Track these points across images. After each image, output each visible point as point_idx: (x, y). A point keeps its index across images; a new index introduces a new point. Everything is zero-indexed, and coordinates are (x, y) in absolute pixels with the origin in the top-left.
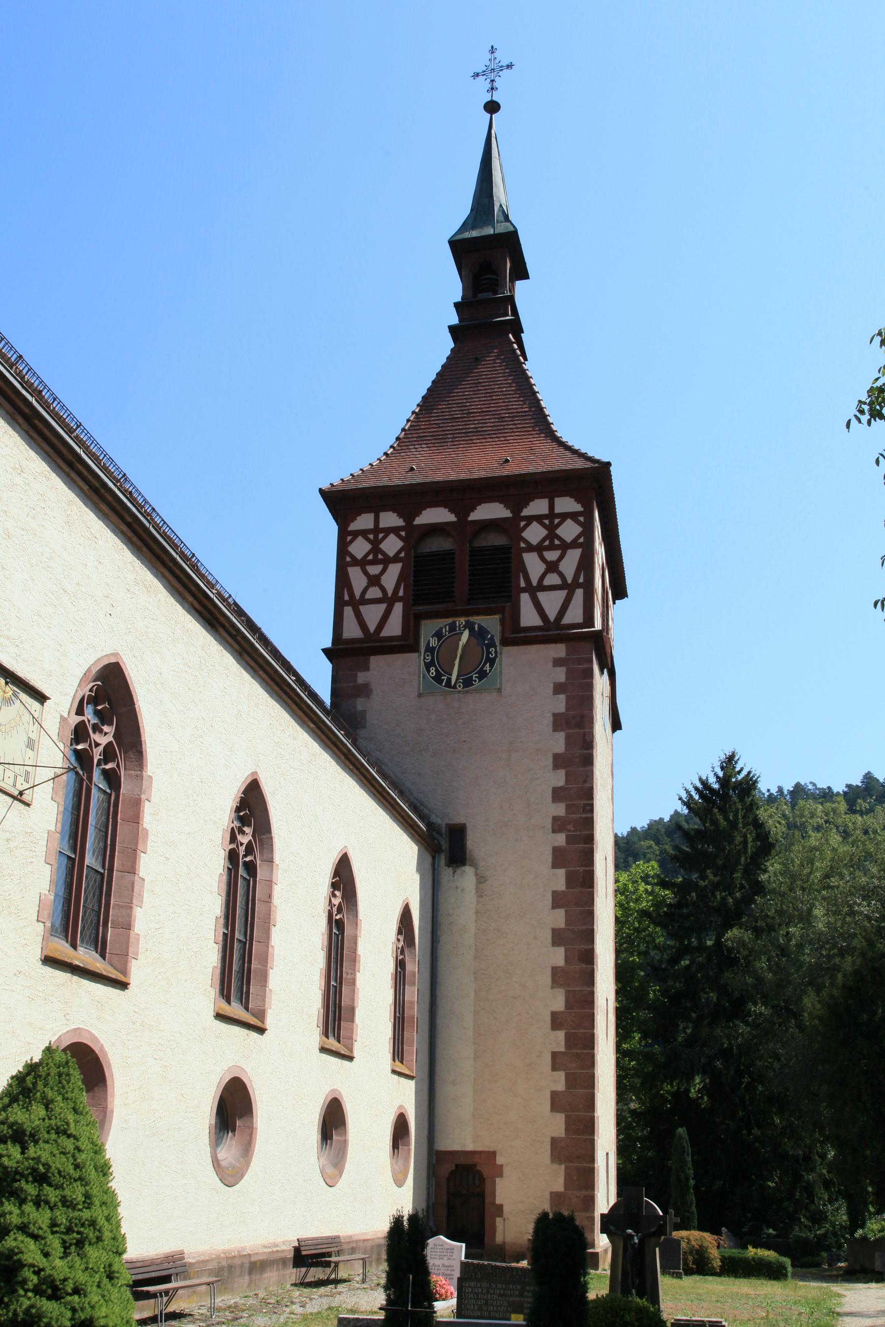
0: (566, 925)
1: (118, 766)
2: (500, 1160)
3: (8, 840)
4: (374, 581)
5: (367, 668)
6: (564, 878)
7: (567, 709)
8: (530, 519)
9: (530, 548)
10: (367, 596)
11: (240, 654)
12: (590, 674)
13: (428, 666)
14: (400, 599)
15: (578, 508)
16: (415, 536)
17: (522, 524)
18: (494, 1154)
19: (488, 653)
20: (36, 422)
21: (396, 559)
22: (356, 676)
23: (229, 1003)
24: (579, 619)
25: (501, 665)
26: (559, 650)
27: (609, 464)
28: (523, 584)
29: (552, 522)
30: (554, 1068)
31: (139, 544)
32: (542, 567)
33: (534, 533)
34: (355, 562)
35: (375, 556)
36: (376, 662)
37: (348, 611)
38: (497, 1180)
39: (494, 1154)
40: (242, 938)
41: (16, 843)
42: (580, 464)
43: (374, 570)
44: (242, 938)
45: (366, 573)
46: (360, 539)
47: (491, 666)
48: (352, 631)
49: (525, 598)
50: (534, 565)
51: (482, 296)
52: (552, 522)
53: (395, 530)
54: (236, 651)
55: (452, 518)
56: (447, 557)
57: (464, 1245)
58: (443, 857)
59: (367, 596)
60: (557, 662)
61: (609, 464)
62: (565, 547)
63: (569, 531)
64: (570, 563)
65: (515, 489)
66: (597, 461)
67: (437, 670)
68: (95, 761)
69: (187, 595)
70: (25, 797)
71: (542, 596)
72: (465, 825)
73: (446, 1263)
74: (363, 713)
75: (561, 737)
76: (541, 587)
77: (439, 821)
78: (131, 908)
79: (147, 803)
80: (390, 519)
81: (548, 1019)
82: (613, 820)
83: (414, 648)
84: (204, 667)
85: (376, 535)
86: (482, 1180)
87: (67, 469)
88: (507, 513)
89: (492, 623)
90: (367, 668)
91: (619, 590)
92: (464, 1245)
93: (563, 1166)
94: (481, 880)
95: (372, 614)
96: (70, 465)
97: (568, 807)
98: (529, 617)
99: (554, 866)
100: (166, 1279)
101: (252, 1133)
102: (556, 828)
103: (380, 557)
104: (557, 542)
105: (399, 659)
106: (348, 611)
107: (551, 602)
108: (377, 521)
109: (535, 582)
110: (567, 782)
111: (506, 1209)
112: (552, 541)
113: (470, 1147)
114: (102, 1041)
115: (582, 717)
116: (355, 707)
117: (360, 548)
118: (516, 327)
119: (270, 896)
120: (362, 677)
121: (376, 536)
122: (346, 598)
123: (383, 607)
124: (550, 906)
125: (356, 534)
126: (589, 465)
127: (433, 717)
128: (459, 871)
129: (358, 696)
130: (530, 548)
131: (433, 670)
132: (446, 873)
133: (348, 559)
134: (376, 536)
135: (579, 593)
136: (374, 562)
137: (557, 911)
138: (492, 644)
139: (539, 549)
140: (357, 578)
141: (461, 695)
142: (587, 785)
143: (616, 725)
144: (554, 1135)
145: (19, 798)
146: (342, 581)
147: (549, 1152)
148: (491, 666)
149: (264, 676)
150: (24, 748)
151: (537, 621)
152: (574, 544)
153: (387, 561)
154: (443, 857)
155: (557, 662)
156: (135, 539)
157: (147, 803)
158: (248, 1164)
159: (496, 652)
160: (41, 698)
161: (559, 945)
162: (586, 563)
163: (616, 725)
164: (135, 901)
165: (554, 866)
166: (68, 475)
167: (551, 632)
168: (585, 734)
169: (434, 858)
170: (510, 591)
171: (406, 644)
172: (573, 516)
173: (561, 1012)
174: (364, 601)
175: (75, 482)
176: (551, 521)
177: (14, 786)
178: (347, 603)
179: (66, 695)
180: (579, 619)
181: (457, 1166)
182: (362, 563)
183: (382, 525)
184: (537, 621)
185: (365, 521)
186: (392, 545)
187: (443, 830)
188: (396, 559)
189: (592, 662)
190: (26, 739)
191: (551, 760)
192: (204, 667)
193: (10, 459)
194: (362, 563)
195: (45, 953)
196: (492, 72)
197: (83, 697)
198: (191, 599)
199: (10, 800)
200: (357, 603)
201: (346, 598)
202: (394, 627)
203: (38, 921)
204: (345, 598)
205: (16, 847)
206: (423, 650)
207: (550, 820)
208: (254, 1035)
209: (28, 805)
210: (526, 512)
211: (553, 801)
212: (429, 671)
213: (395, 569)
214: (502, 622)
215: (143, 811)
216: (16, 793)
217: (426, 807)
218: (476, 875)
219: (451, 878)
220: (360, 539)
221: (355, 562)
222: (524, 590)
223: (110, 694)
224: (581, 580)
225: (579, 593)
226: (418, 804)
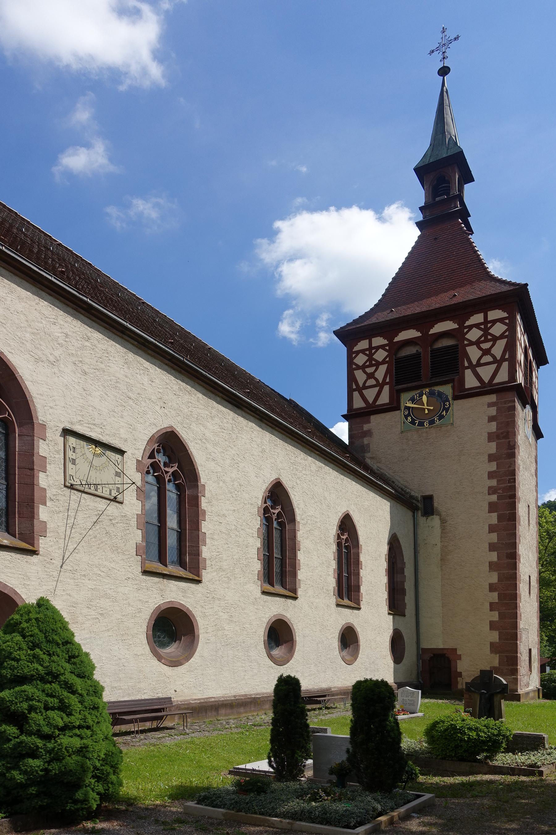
0: (498, 540)
1: (183, 481)
2: (459, 652)
3: (110, 520)
4: (371, 376)
5: (369, 422)
6: (496, 517)
7: (497, 429)
8: (470, 327)
9: (471, 343)
10: (367, 385)
11: (261, 420)
12: (513, 408)
13: (406, 417)
14: (387, 384)
15: (505, 315)
16: (394, 348)
17: (465, 330)
18: (456, 649)
19: (444, 405)
20: (93, 311)
21: (383, 362)
22: (362, 427)
23: (274, 587)
24: (506, 379)
25: (453, 410)
26: (493, 398)
27: (526, 285)
28: (466, 364)
29: (486, 326)
30: (491, 610)
31: (179, 369)
32: (493, 351)
33: (474, 335)
34: (358, 367)
35: (371, 362)
36: (373, 418)
37: (356, 394)
38: (458, 661)
39: (456, 649)
40: (279, 556)
41: (116, 521)
42: (505, 288)
43: (370, 370)
44: (279, 556)
45: (365, 372)
46: (361, 355)
47: (447, 412)
48: (358, 403)
49: (468, 373)
50: (474, 353)
51: (437, 199)
52: (486, 326)
53: (382, 347)
54: (258, 419)
55: (419, 334)
56: (417, 356)
57: (420, 691)
58: (420, 512)
59: (367, 385)
60: (490, 405)
61: (526, 285)
62: (495, 339)
63: (498, 329)
64: (498, 349)
65: (460, 312)
66: (510, 283)
67: (412, 418)
68: (167, 480)
69: (218, 393)
70: (117, 500)
71: (479, 370)
72: (432, 495)
73: (411, 699)
74: (368, 445)
75: (494, 445)
76: (479, 364)
77: (417, 495)
78: (199, 547)
79: (203, 498)
80: (378, 341)
81: (488, 587)
82: (537, 486)
83: (398, 408)
84: (235, 429)
85: (370, 351)
86: (449, 661)
87: (121, 335)
88: (456, 326)
89: (447, 390)
90: (369, 422)
91: (541, 359)
92: (420, 691)
93: (498, 655)
94: (443, 521)
95: (370, 394)
96: (122, 332)
97: (498, 481)
98: (471, 381)
99: (490, 512)
100: (325, 696)
101: (293, 644)
102: (491, 492)
103: (374, 362)
104: (489, 337)
105: (388, 416)
106: (356, 394)
107: (486, 373)
108: (370, 343)
109: (361, 385)
110: (497, 468)
111: (463, 674)
112: (487, 336)
113: (441, 646)
114: (188, 606)
115: (508, 432)
116: (363, 442)
117: (361, 360)
118: (464, 214)
119: (295, 537)
120: (366, 427)
121: (370, 352)
122: (354, 387)
123: (377, 389)
124: (488, 532)
125: (358, 353)
126: (512, 288)
127: (410, 442)
128: (430, 518)
129: (365, 437)
130: (471, 343)
131: (409, 418)
132: (422, 520)
133: (354, 366)
134: (370, 352)
135: (505, 365)
136: (371, 366)
137: (491, 534)
138: (448, 400)
139: (477, 343)
140: (360, 376)
141: (428, 430)
142: (511, 469)
143: (538, 434)
144: (492, 641)
145: (115, 500)
146: (351, 378)
147: (489, 649)
148: (447, 412)
149: (279, 430)
150: (114, 477)
151: (477, 384)
152: (502, 337)
153: (378, 364)
154: (420, 512)
155: (490, 405)
156: (175, 367)
157: (203, 498)
158: (292, 656)
159: (449, 404)
160: (121, 452)
161: (494, 551)
162: (511, 347)
163: (538, 434)
164: (200, 543)
165: (490, 512)
166: (122, 338)
167: (485, 389)
168: (509, 442)
169: (414, 513)
170: (458, 370)
171: (393, 406)
172: (501, 320)
173: (496, 583)
174: (365, 387)
175: (128, 341)
176: (485, 326)
177: (110, 494)
178: (355, 390)
179: (139, 449)
180: (506, 379)
181: (434, 655)
182: (363, 368)
183: (490, 318)
184: (477, 384)
185: (363, 344)
186: (380, 355)
187: (419, 499)
188: (383, 362)
189: (514, 401)
190: (114, 472)
191: (487, 457)
192: (235, 429)
193: (79, 333)
194: (363, 368)
195: (143, 569)
196: (442, 48)
197: (154, 449)
198: (221, 395)
199: (108, 502)
200: (360, 390)
201: (354, 387)
202: (385, 398)
203: (137, 555)
204: (353, 386)
205: (117, 523)
206: (403, 408)
207: (487, 488)
208: (290, 601)
209: (122, 503)
210: (467, 323)
211: (489, 479)
212: (407, 419)
213: (383, 369)
214: (453, 388)
215: (201, 501)
216: (112, 498)
217: (408, 488)
218: (440, 519)
219: (425, 522)
220: (361, 355)
221: (358, 367)
222: (467, 368)
223: (170, 448)
224: (507, 357)
225: (505, 365)
226: (403, 487)
